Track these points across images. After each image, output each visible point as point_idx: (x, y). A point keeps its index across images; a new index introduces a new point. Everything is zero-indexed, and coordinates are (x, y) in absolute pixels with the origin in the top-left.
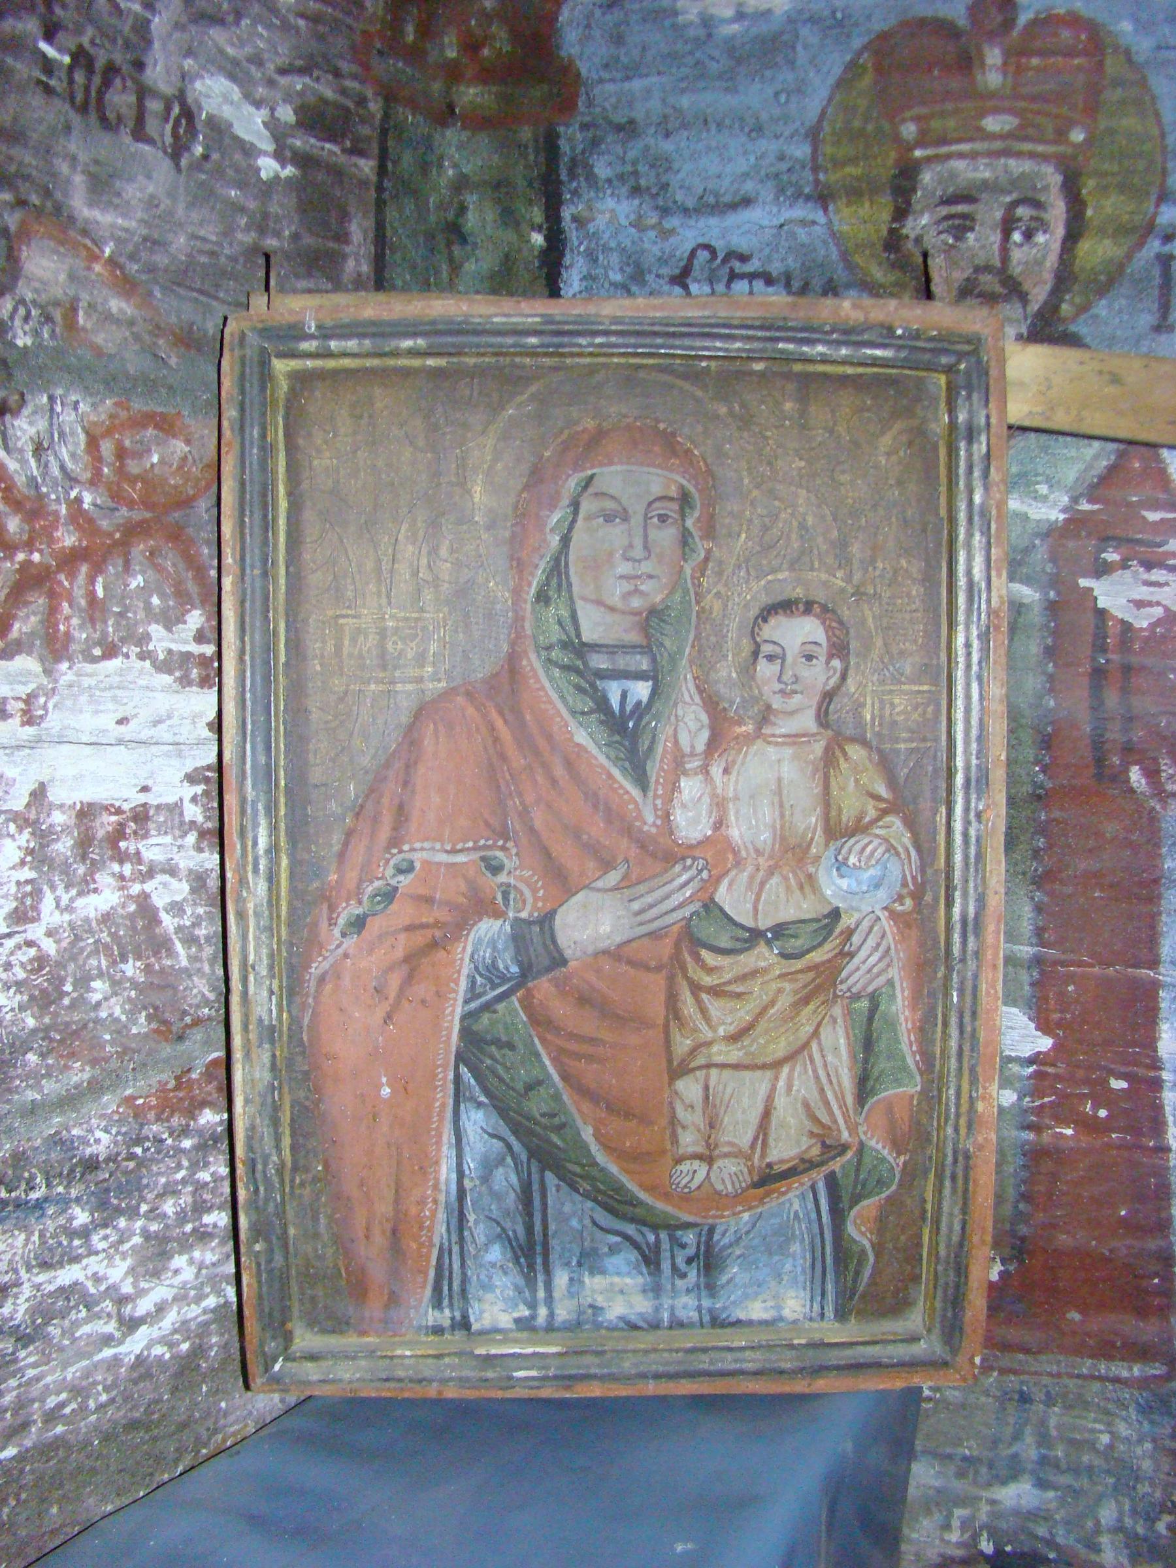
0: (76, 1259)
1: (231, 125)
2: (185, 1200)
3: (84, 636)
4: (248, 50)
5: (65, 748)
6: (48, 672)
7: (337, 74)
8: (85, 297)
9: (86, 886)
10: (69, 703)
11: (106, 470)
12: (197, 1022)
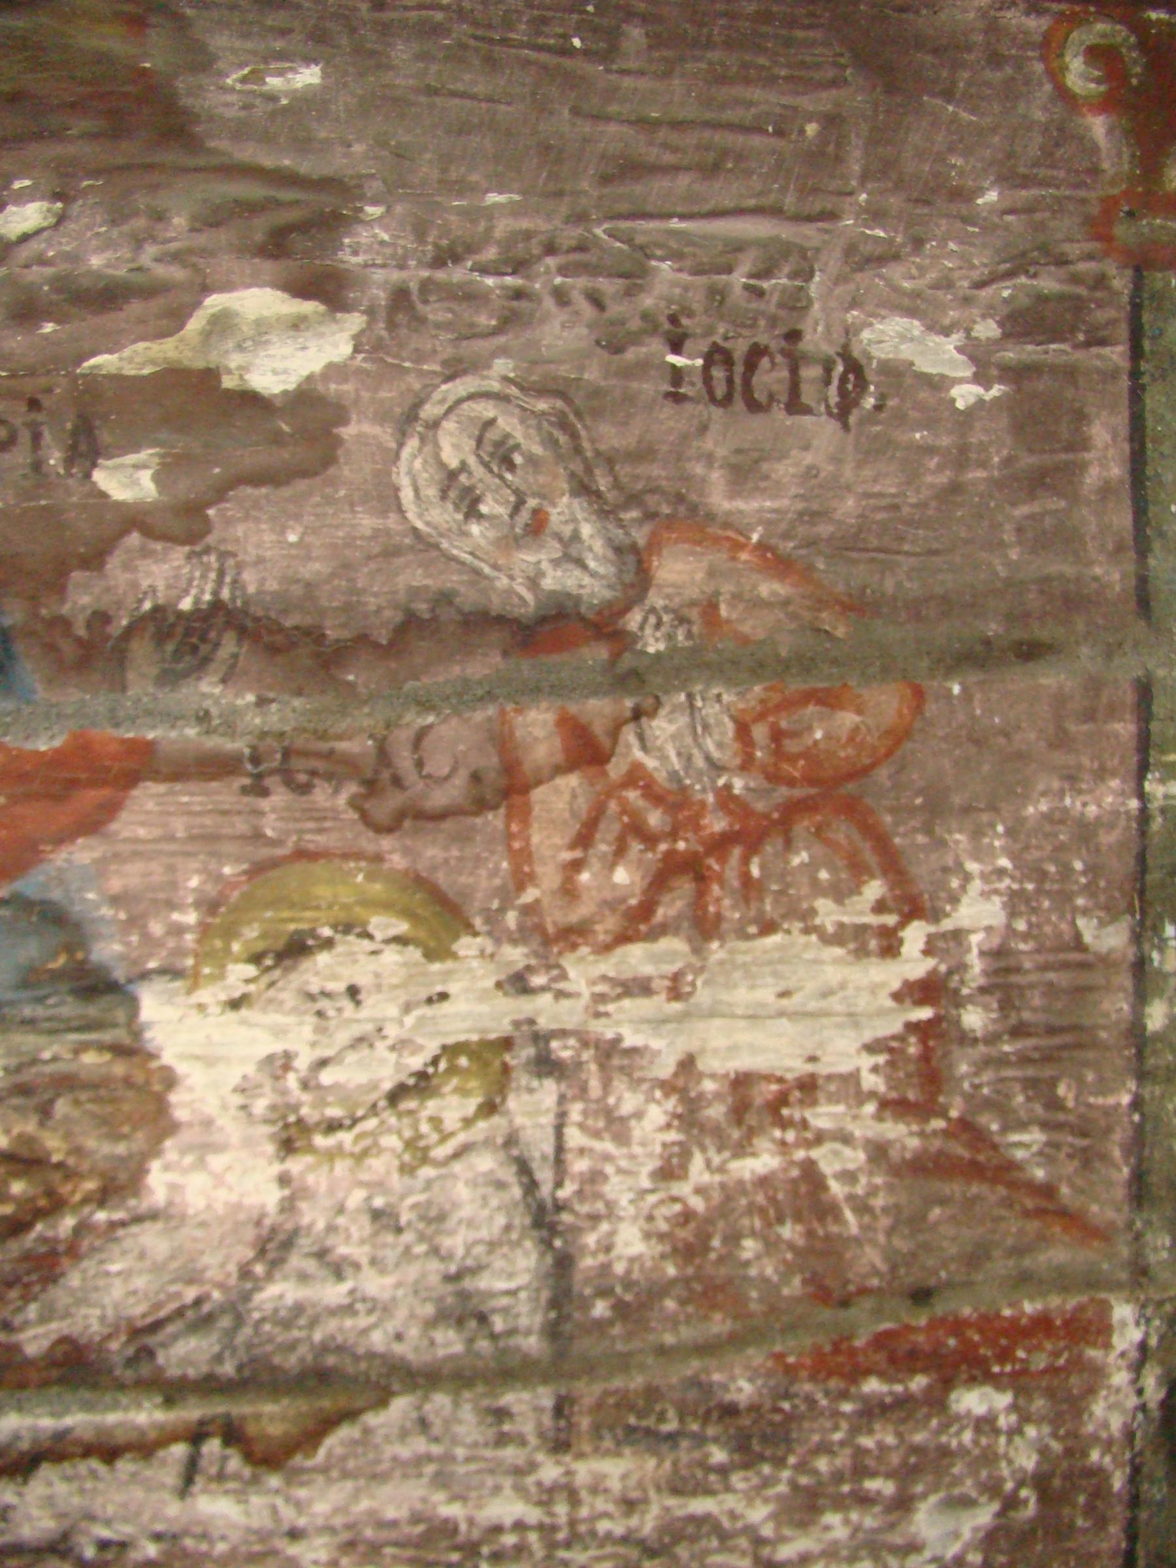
0: (709, 1492)
1: (912, 364)
2: (843, 1460)
3: (737, 915)
4: (931, 276)
5: (717, 1022)
6: (696, 951)
7: (1062, 261)
8: (727, 588)
9: (742, 1149)
10: (721, 980)
11: (759, 754)
12: (863, 1291)
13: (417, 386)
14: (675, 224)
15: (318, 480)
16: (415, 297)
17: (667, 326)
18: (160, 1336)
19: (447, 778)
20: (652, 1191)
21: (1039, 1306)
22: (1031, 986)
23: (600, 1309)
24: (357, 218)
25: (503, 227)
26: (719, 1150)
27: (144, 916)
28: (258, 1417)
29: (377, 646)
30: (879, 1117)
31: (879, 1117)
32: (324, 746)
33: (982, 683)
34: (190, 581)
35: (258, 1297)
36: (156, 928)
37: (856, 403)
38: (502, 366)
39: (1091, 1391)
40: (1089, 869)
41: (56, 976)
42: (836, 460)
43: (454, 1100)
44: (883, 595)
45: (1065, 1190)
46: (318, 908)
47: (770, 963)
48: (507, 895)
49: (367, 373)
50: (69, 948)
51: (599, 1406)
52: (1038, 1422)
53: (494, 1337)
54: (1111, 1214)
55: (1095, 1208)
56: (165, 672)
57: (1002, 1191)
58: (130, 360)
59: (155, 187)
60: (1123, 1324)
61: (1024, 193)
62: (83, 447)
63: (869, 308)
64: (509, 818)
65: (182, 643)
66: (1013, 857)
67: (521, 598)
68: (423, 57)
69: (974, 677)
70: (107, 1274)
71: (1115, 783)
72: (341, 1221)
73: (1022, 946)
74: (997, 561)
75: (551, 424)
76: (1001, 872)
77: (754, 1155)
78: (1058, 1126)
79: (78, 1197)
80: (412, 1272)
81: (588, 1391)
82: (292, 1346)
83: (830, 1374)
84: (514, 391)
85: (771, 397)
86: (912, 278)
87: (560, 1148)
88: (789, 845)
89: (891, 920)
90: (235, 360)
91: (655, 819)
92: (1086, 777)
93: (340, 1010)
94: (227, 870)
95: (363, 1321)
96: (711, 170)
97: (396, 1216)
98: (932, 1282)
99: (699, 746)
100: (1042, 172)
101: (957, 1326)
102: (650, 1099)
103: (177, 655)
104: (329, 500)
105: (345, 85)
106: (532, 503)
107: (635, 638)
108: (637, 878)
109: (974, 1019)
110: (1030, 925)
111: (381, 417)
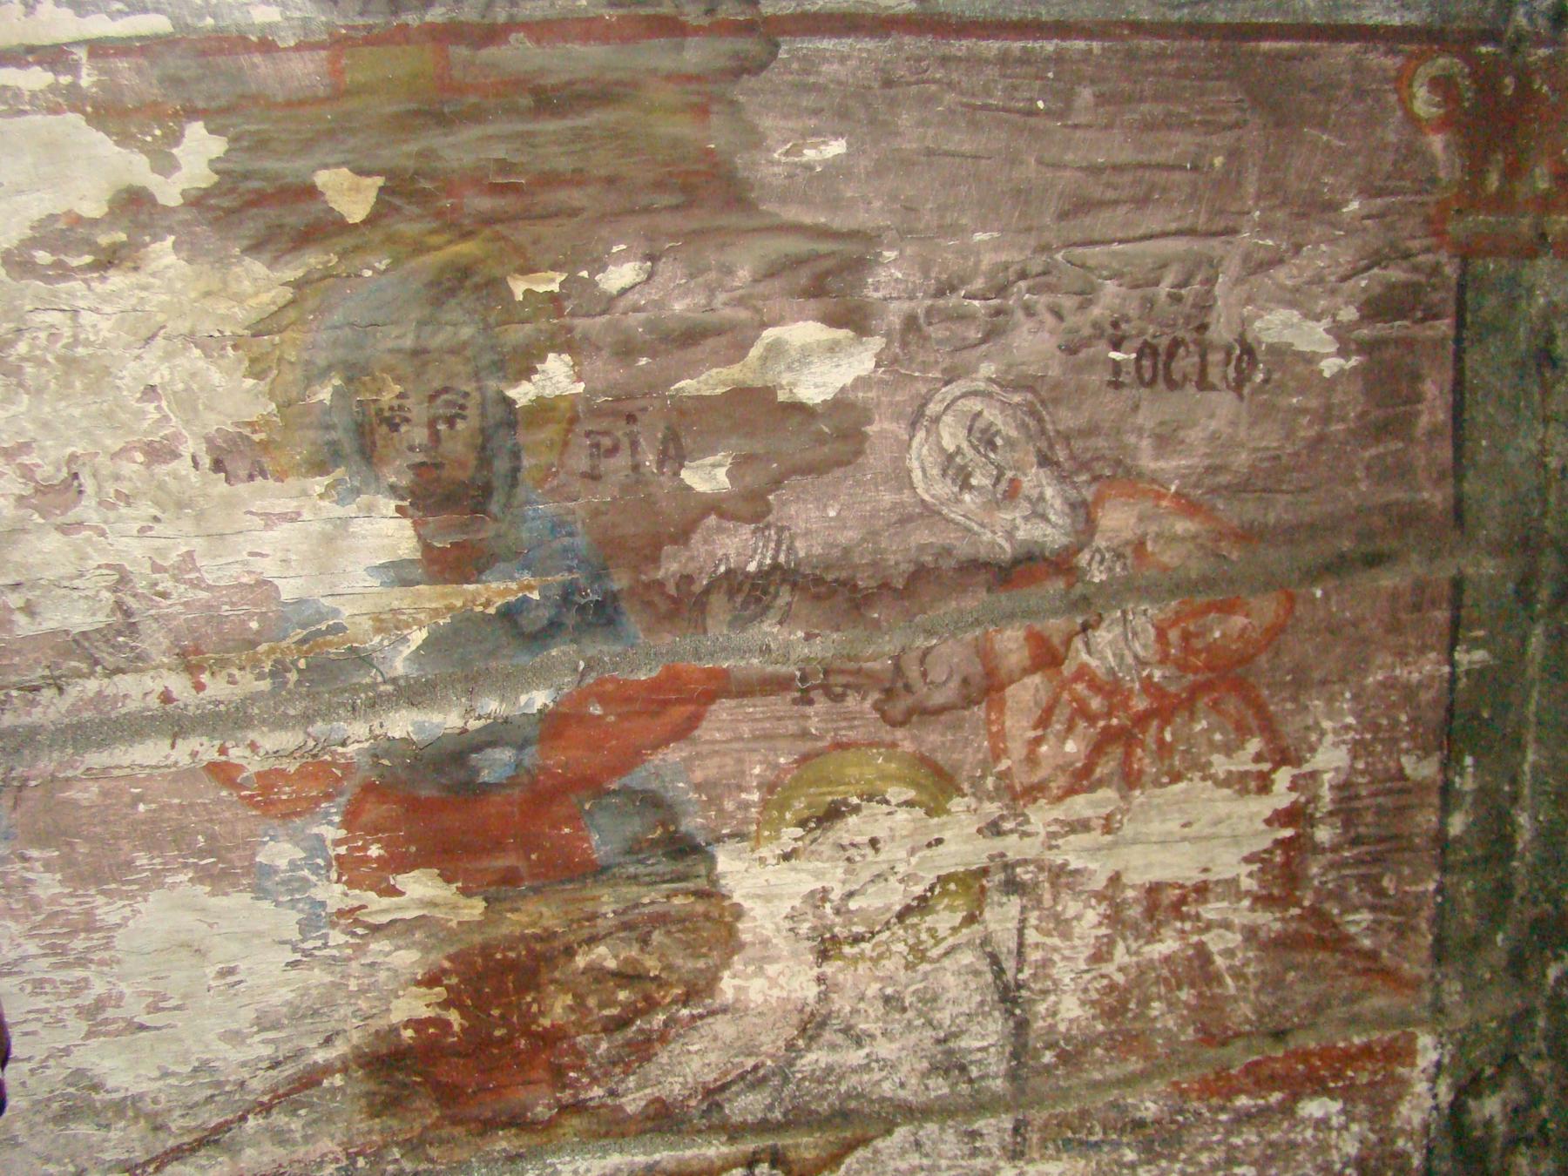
2: (1219, 1155)
4: (1307, 274)
5: (1138, 847)
6: (1123, 797)
9: (1152, 938)
12: (1238, 1035)
13: (924, 390)
14: (1116, 247)
15: (850, 468)
16: (922, 320)
17: (1110, 331)
18: (727, 1094)
19: (945, 683)
20: (1087, 971)
21: (1364, 1039)
22: (1367, 808)
23: (1048, 1057)
24: (877, 261)
25: (987, 260)
26: (1136, 939)
27: (720, 797)
28: (797, 1146)
29: (895, 590)
30: (1252, 909)
31: (1252, 909)
32: (852, 665)
33: (1336, 588)
34: (755, 551)
35: (799, 1063)
36: (729, 805)
37: (1249, 379)
38: (988, 369)
39: (1399, 1097)
40: (1412, 721)
41: (654, 844)
42: (1234, 423)
43: (945, 915)
44: (1266, 526)
45: (1385, 953)
46: (849, 784)
47: (1177, 803)
48: (986, 766)
49: (887, 383)
50: (664, 824)
51: (1046, 1125)
52: (1359, 1121)
53: (971, 1081)
54: (1418, 970)
55: (1406, 966)
56: (736, 618)
57: (1339, 956)
58: (706, 383)
59: (722, 247)
60: (1425, 1048)
61: (1379, 201)
62: (672, 452)
63: (1260, 302)
64: (989, 709)
65: (749, 594)
66: (1359, 715)
67: (1001, 547)
68: (922, 123)
69: (1331, 583)
70: (689, 1052)
71: (1432, 655)
72: (862, 1006)
73: (1361, 780)
74: (1350, 494)
75: (1025, 413)
76: (1347, 728)
77: (1160, 941)
78: (1384, 908)
79: (668, 1000)
80: (913, 1038)
81: (1038, 1116)
82: (823, 1097)
83: (1212, 1095)
84: (995, 388)
85: (1185, 378)
86: (1292, 277)
87: (1021, 945)
88: (1192, 717)
89: (1266, 767)
90: (786, 379)
91: (1096, 703)
92: (1412, 652)
93: (864, 856)
94: (782, 760)
95: (877, 1076)
96: (1142, 202)
97: (903, 1001)
98: (1288, 1025)
99: (1129, 648)
100: (1392, 184)
101: (1305, 1056)
102: (1088, 906)
103: (745, 605)
104: (858, 483)
105: (864, 152)
106: (1009, 474)
107: (1085, 572)
108: (1082, 748)
109: (1323, 834)
110: (1367, 764)
111: (897, 417)
